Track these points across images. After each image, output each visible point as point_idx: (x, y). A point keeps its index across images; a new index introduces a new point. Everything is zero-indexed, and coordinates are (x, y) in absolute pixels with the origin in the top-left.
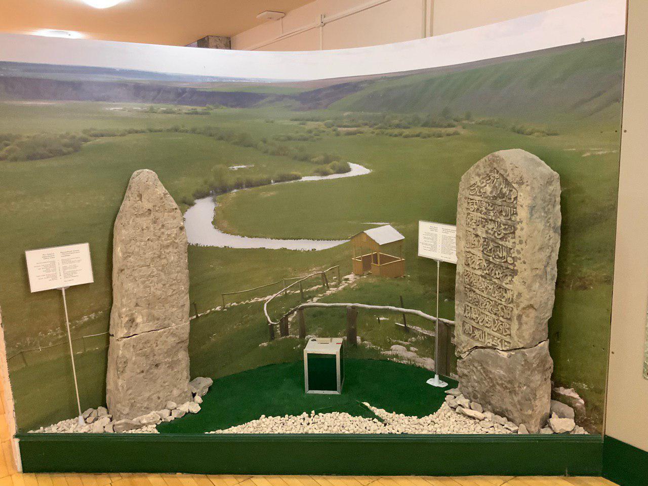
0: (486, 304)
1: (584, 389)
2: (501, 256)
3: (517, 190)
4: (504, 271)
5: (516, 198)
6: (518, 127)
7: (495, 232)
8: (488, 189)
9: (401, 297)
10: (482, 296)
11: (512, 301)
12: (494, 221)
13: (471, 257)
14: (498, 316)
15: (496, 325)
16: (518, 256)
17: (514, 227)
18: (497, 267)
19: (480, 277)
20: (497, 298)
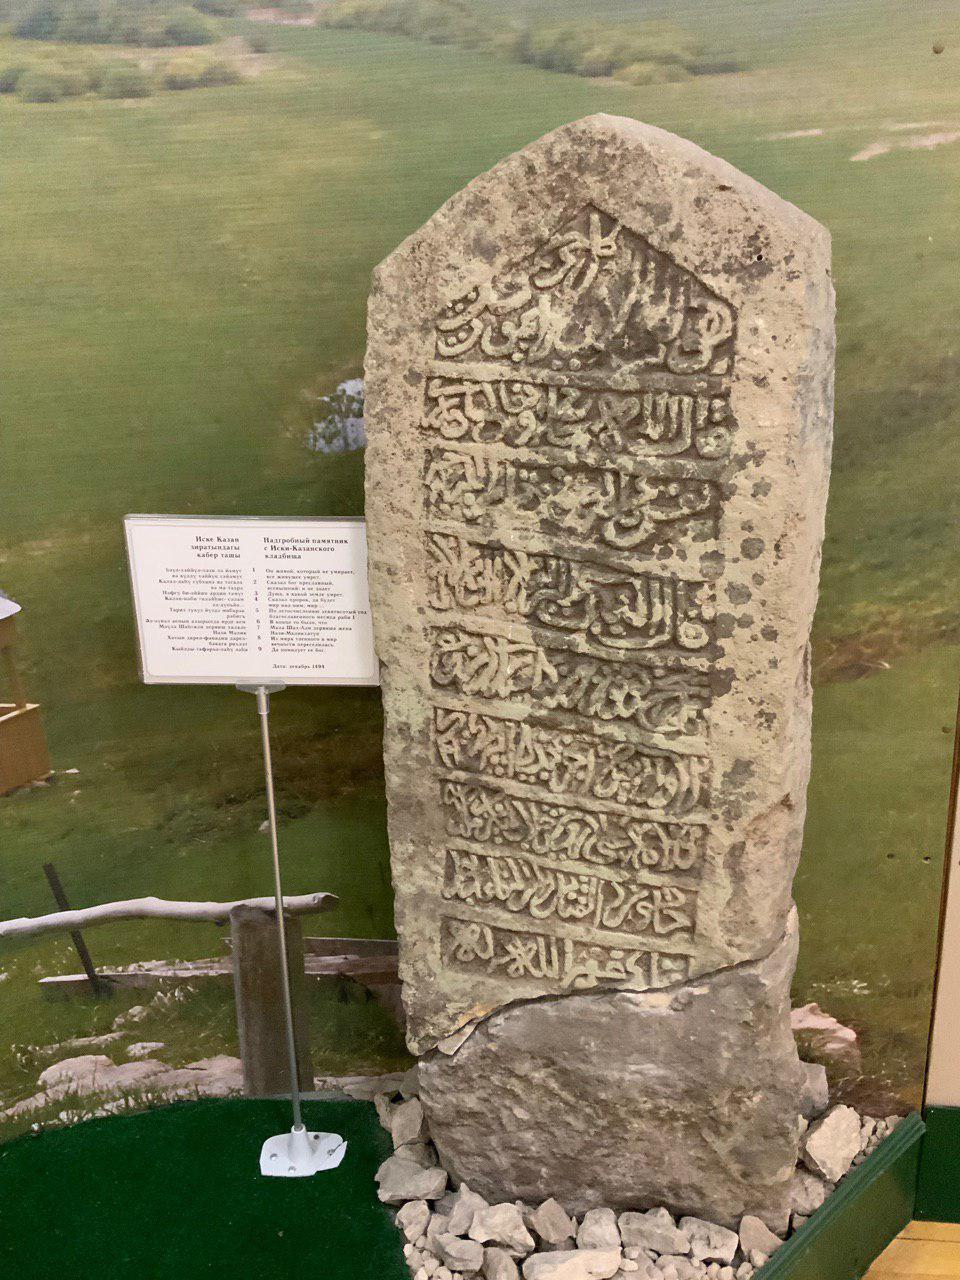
0: (565, 833)
1: (856, 996)
2: (638, 621)
3: (736, 303)
4: (660, 683)
5: (726, 348)
6: (546, 37)
7: (601, 520)
8: (552, 319)
9: (49, 869)
10: (539, 803)
11: (705, 801)
12: (595, 473)
13: (464, 650)
14: (630, 866)
15: (617, 903)
16: (738, 612)
17: (716, 486)
18: (616, 673)
19: (526, 727)
20: (623, 798)
